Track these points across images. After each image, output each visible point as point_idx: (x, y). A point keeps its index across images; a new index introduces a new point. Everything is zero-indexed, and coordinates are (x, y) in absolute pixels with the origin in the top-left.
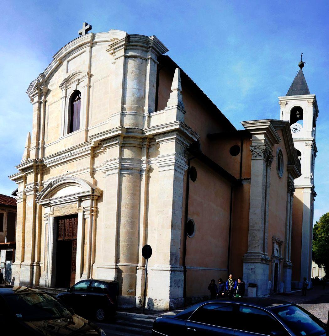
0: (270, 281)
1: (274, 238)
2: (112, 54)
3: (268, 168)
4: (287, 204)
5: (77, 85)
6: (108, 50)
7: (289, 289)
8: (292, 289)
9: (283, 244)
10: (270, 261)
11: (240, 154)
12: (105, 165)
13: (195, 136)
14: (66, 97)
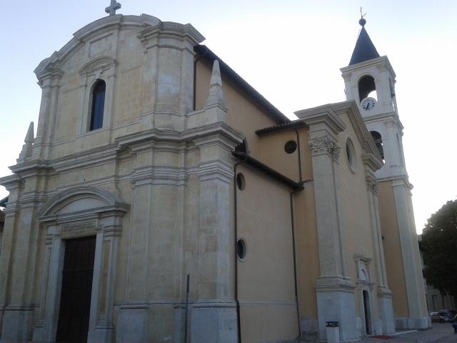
0: (360, 317)
1: (356, 256)
2: (142, 42)
3: (335, 164)
4: (370, 207)
5: (101, 73)
6: (139, 37)
7: (391, 330)
8: (397, 330)
9: (372, 262)
10: (353, 288)
11: (296, 151)
12: (134, 174)
13: (240, 138)
14: (86, 86)
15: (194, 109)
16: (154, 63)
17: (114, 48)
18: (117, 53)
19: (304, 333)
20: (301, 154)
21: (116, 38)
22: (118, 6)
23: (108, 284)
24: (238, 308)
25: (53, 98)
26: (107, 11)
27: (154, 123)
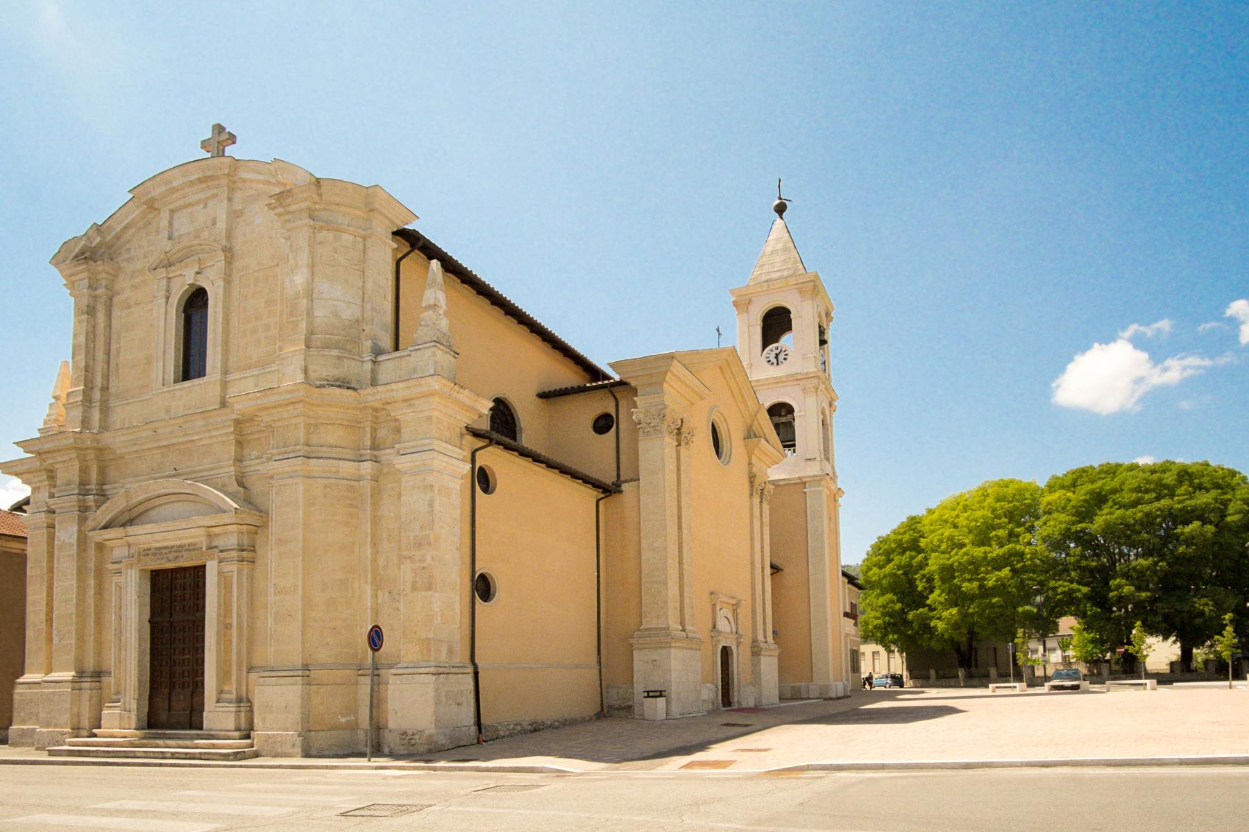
2: (279, 215)
11: (614, 428)
15: (397, 348)
16: (304, 258)
17: (222, 225)
18: (229, 234)
19: (610, 707)
20: (621, 434)
21: (225, 204)
22: (232, 139)
23: (234, 640)
24: (476, 674)
25: (101, 316)
26: (205, 145)
27: (306, 371)
